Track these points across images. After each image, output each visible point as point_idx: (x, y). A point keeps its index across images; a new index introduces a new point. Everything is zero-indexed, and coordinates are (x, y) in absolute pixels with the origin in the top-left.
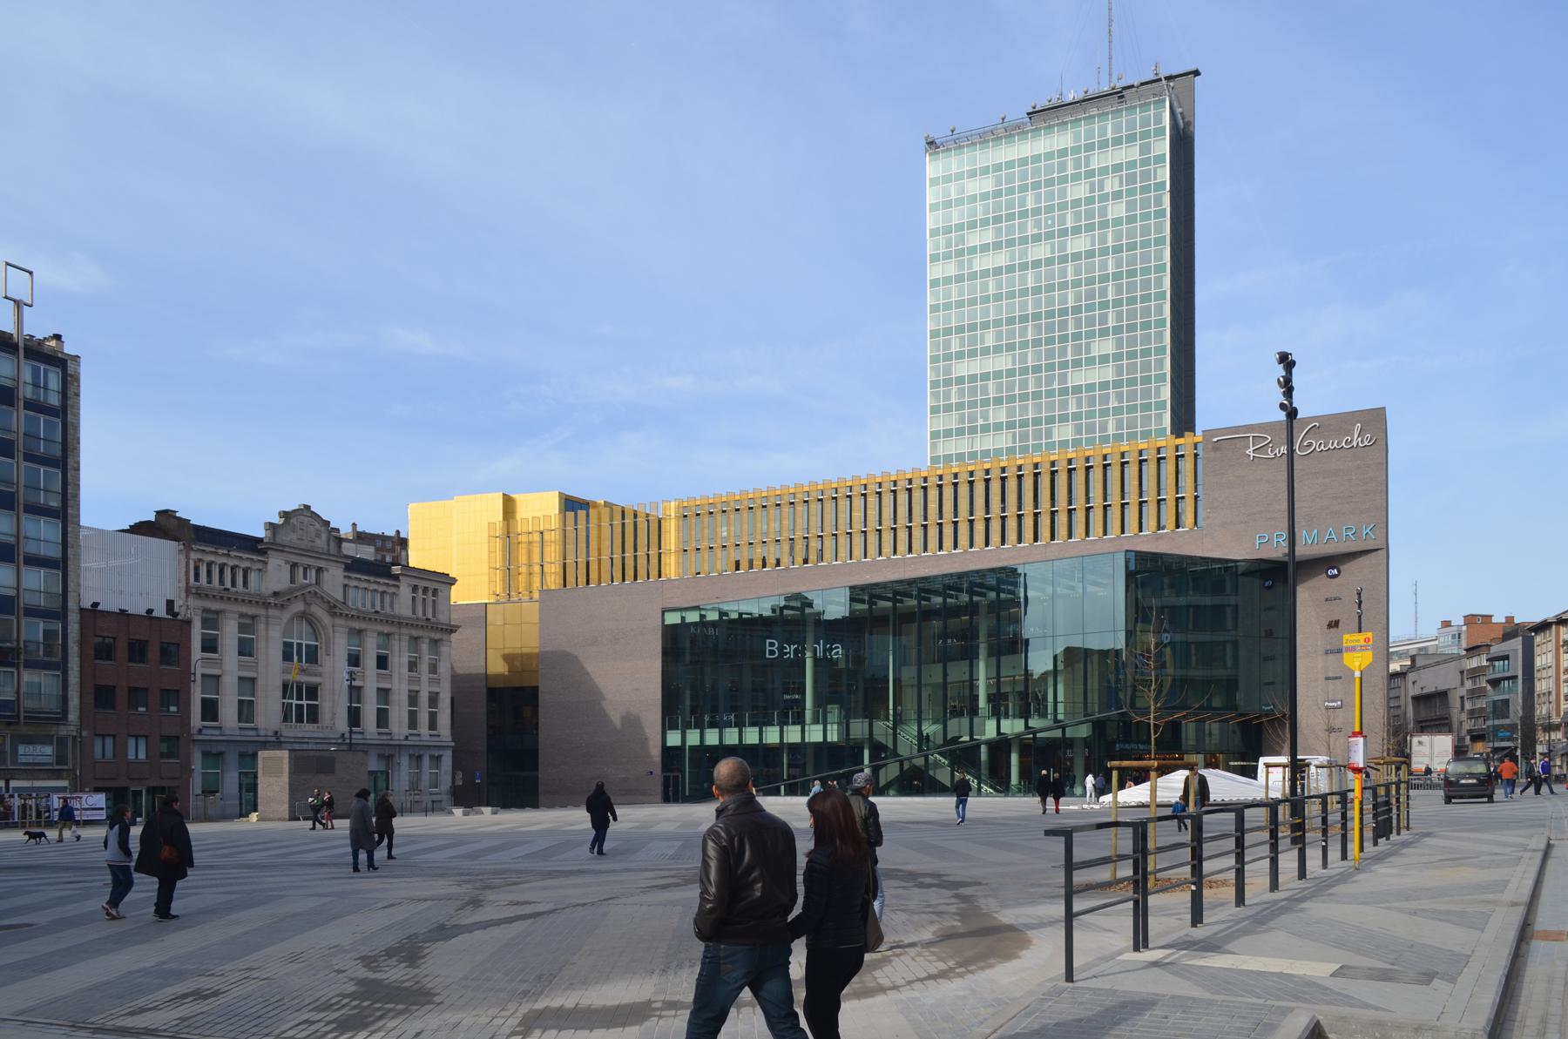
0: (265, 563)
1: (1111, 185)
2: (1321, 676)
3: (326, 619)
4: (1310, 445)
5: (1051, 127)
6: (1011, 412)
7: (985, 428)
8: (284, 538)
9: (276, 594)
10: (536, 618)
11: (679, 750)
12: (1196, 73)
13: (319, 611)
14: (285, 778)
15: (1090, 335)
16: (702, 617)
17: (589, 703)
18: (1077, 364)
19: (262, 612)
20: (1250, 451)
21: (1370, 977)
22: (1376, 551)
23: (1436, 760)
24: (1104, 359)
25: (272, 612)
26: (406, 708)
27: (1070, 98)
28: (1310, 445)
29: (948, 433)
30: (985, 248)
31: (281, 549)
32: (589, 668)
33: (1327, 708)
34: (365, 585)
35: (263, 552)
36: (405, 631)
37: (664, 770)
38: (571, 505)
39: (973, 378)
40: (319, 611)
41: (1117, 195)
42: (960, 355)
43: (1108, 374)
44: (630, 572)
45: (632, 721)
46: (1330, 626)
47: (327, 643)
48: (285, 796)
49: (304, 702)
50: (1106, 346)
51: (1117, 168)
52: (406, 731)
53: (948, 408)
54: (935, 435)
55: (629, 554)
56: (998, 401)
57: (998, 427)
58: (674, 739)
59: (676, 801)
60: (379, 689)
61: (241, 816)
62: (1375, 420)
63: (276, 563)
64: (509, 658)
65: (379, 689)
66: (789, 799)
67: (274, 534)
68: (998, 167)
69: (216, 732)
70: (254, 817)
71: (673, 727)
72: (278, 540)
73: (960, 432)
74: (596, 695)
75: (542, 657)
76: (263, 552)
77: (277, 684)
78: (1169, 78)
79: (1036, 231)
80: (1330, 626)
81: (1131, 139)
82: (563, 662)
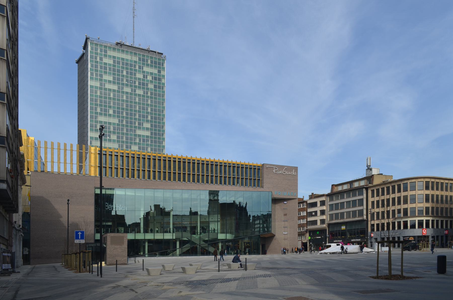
18: (139, 128)
24: (147, 129)
30: (110, 82)
41: (151, 82)
42: (101, 114)
43: (148, 133)
51: (151, 74)
56: (114, 133)
57: (114, 141)
68: (114, 57)
78: (158, 53)
79: (127, 83)
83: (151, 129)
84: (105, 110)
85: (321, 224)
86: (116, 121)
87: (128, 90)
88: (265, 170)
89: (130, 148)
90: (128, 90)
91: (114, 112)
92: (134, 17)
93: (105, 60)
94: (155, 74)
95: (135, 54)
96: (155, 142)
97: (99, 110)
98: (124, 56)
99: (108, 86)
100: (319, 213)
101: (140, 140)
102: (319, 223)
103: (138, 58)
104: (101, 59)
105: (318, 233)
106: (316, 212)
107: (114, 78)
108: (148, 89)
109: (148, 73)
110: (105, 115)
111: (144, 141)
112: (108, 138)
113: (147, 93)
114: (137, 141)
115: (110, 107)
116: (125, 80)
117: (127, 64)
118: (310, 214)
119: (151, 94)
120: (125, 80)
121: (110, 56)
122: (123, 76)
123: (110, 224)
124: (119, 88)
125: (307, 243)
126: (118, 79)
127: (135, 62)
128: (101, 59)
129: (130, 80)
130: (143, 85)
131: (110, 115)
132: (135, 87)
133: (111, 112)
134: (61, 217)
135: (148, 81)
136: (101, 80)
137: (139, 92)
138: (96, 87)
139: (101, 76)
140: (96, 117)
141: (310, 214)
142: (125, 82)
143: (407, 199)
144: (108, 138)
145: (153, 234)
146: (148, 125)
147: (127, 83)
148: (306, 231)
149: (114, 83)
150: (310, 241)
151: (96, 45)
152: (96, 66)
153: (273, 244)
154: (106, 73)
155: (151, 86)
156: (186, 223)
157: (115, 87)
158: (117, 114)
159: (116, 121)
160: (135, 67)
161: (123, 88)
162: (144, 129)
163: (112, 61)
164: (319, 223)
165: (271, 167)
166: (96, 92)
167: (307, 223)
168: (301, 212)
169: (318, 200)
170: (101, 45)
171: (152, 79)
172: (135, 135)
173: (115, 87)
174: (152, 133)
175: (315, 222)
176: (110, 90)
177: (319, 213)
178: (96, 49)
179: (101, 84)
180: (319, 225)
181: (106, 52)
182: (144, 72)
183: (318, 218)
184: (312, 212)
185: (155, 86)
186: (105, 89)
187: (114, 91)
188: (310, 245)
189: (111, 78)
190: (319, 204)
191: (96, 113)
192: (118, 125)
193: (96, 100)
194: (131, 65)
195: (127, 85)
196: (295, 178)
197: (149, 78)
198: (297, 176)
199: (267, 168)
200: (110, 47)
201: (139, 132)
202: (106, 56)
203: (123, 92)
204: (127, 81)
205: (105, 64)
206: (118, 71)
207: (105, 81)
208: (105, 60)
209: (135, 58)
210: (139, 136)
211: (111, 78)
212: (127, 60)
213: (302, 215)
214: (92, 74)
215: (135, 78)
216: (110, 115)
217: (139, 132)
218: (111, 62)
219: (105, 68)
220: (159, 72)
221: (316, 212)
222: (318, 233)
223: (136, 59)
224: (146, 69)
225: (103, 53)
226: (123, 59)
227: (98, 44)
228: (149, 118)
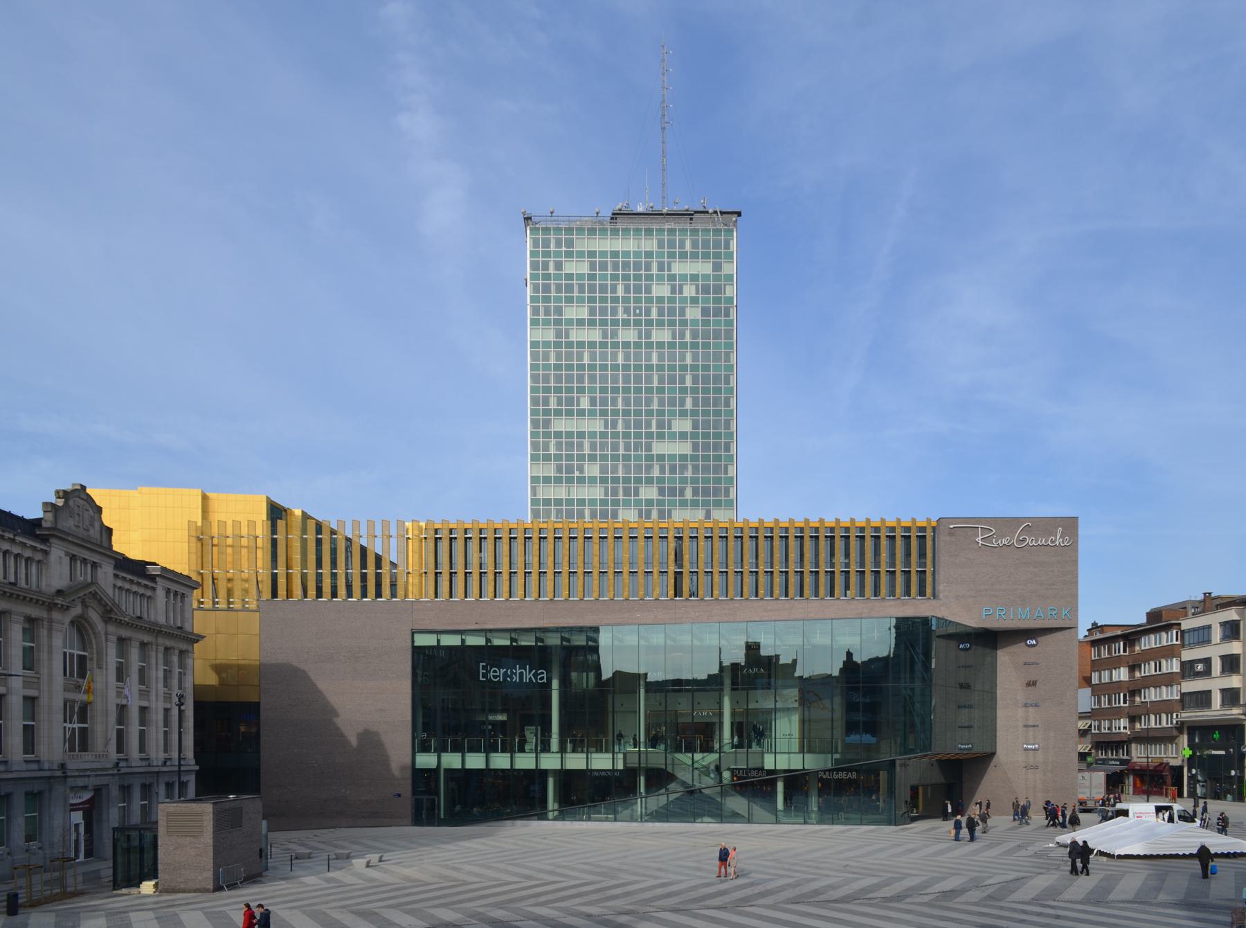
0: (46, 553)
1: (689, 290)
2: (1020, 724)
3: (100, 626)
4: (1024, 540)
5: (626, 231)
6: (603, 469)
7: (581, 480)
8: (68, 524)
9: (59, 592)
10: (256, 630)
11: (432, 774)
12: (739, 214)
13: (94, 616)
14: (208, 837)
15: (672, 413)
16: (463, 641)
17: (321, 719)
18: (661, 436)
19: (42, 614)
20: (979, 539)
21: (91, 836)
22: (1076, 627)
23: (1094, 791)
24: (683, 435)
25: (56, 615)
26: (162, 729)
27: (640, 209)
28: (1024, 540)
29: (547, 480)
30: (581, 322)
31: (64, 537)
32: (322, 685)
33: (1026, 750)
34: (127, 586)
35: (45, 539)
36: (160, 641)
37: (414, 792)
38: (276, 513)
39: (570, 434)
40: (94, 616)
41: (694, 300)
42: (558, 413)
43: (685, 448)
44: (327, 588)
45: (370, 740)
46: (1028, 684)
47: (99, 653)
48: (208, 861)
49: (76, 726)
50: (685, 425)
51: (694, 277)
52: (162, 755)
53: (547, 458)
54: (535, 480)
55: (326, 570)
56: (592, 458)
57: (592, 480)
58: (426, 760)
59: (430, 823)
60: (25, 698)
61: (116, 885)
62: (1070, 525)
63: (57, 553)
64: (218, 669)
65: (25, 698)
66: (560, 825)
67: (56, 517)
68: (592, 254)
69: (35, 766)
70: (147, 887)
71: (425, 749)
72: (60, 527)
73: (558, 480)
74: (330, 712)
75: (264, 671)
76: (45, 539)
77: (58, 703)
78: (722, 213)
79: (625, 316)
80: (1028, 684)
81: (706, 256)
82: (288, 677)
83: (694, 435)
84: (570, 401)
85: (1223, 704)
86: (597, 425)
87: (629, 335)
88: (943, 539)
89: (636, 494)
90: (629, 335)
91: (593, 402)
92: (664, 129)
93: (571, 267)
94: (706, 277)
95: (649, 232)
96: (706, 469)
97: (553, 405)
98: (618, 244)
99: (576, 335)
100: (1217, 666)
101: (662, 470)
102: (1217, 699)
103: (655, 242)
104: (558, 266)
105: (1216, 736)
106: (1207, 662)
107: (592, 311)
108: (684, 323)
109: (683, 277)
110: (570, 413)
111: (673, 469)
112: (577, 474)
113: (682, 335)
114: (656, 473)
115: (581, 390)
116: (620, 310)
117: (626, 265)
118: (1189, 669)
119: (694, 334)
120: (620, 310)
121: (581, 254)
122: (615, 300)
123: (502, 717)
124: (605, 335)
125: (1181, 768)
126: (603, 311)
127: (649, 254)
128: (558, 266)
129: (635, 309)
130: (671, 315)
131: (581, 413)
132: (649, 323)
133: (585, 403)
134: (337, 715)
135: (683, 300)
136: (558, 322)
137: (662, 335)
138: (547, 344)
139: (559, 311)
140: (547, 423)
141: (1189, 669)
142: (621, 316)
143: (785, 799)
144: (577, 474)
145: (584, 755)
146: (685, 425)
147: (625, 316)
148: (1180, 727)
149: (592, 323)
150: (1191, 759)
151: (546, 230)
152: (547, 289)
153: (989, 787)
154: (569, 300)
155: (693, 313)
156: (705, 713)
157: (595, 335)
158: (601, 409)
159: (597, 425)
160: (648, 267)
161: (615, 334)
162: (672, 436)
163: (586, 265)
164: (1217, 699)
165: (964, 529)
166: (546, 357)
167: (1182, 700)
168: (1164, 662)
169: (1214, 620)
170: (558, 230)
171: (697, 292)
172: (650, 458)
173: (595, 335)
174: (695, 447)
175: (1203, 699)
176: (581, 344)
177: (1217, 666)
178: (546, 244)
179: (558, 334)
180: (1217, 710)
181: (570, 243)
182: (672, 277)
183: (1216, 684)
184: (1192, 663)
185: (705, 312)
186: (570, 345)
187: (592, 344)
188: (1192, 778)
189: (584, 314)
190: (1217, 634)
191: (547, 412)
192: (603, 435)
193: (546, 379)
194: (637, 266)
195: (626, 323)
196: (1068, 557)
197: (689, 290)
198: (1074, 546)
199: (952, 532)
200: (580, 230)
201: (659, 448)
202: (569, 254)
203: (615, 345)
204: (627, 311)
205: (569, 276)
206: (603, 288)
207: (570, 322)
208: (571, 267)
209: (648, 242)
210: (661, 457)
211: (584, 314)
212: (626, 254)
213: (1164, 670)
214: (535, 311)
215: (649, 300)
216: (581, 413)
217: (659, 448)
218: (584, 268)
219: (569, 288)
220: (717, 267)
221: (1207, 662)
222: (1216, 736)
223: (650, 245)
224: (678, 268)
225: (564, 249)
226: (615, 254)
227: (549, 229)
228: (689, 405)
